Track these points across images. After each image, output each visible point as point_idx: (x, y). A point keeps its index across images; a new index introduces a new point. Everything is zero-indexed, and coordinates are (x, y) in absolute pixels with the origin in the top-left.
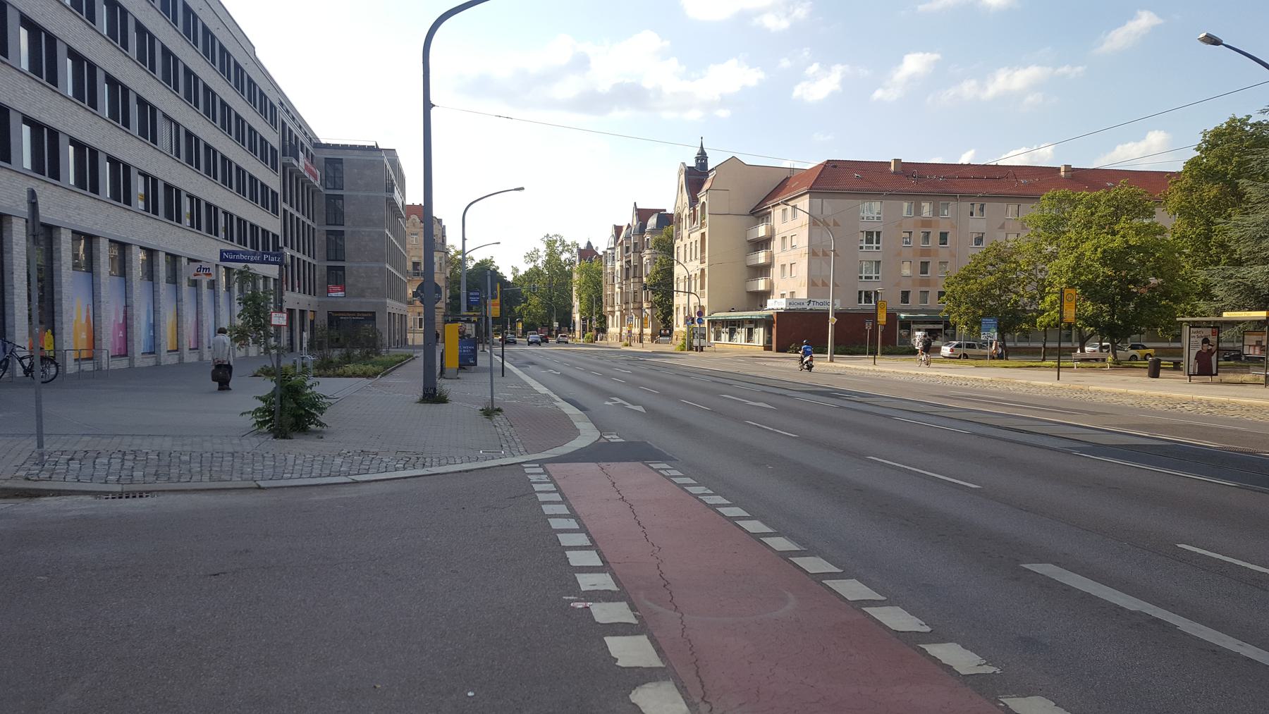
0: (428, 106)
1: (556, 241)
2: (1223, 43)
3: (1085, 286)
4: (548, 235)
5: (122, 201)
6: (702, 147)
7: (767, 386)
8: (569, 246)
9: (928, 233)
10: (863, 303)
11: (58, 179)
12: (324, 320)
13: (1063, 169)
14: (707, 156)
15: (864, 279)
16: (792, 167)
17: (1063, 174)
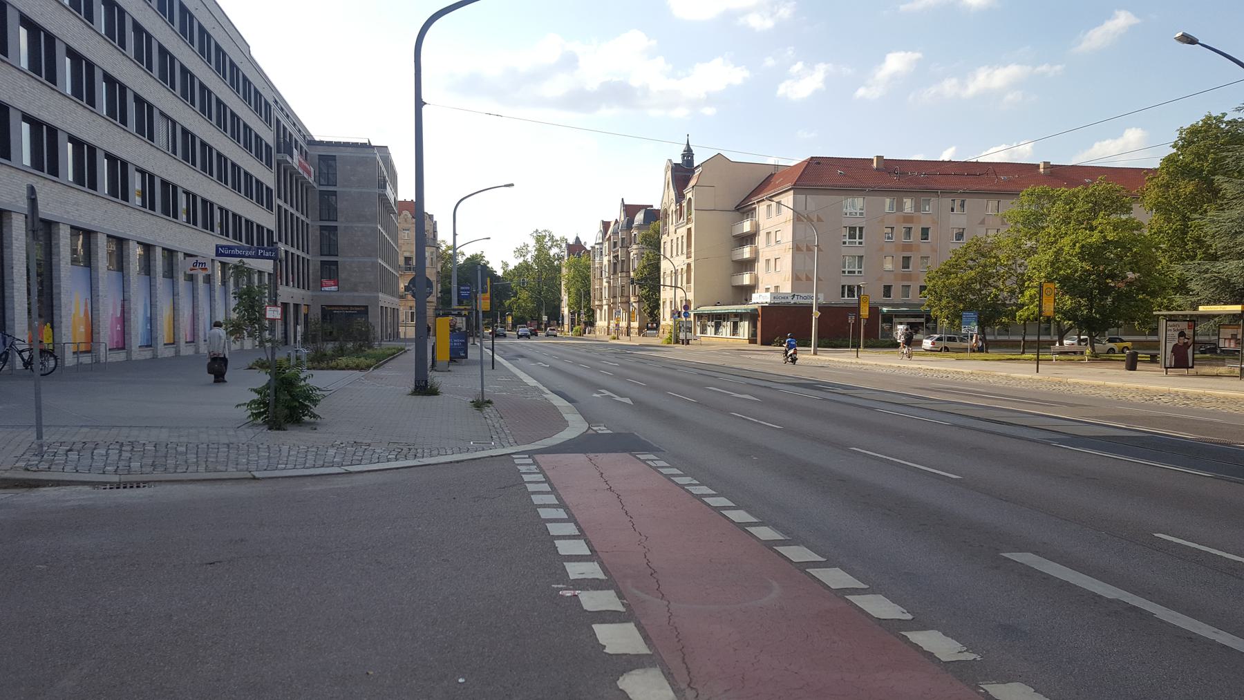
0: (419, 103)
1: (545, 236)
2: (1199, 42)
3: (1064, 281)
4: (537, 230)
5: (120, 197)
6: (688, 144)
7: (752, 378)
8: (557, 241)
9: (910, 228)
10: (846, 297)
11: (57, 176)
12: (317, 314)
13: (1042, 166)
14: (693, 152)
15: (847, 274)
16: (776, 164)
17: (1042, 170)
